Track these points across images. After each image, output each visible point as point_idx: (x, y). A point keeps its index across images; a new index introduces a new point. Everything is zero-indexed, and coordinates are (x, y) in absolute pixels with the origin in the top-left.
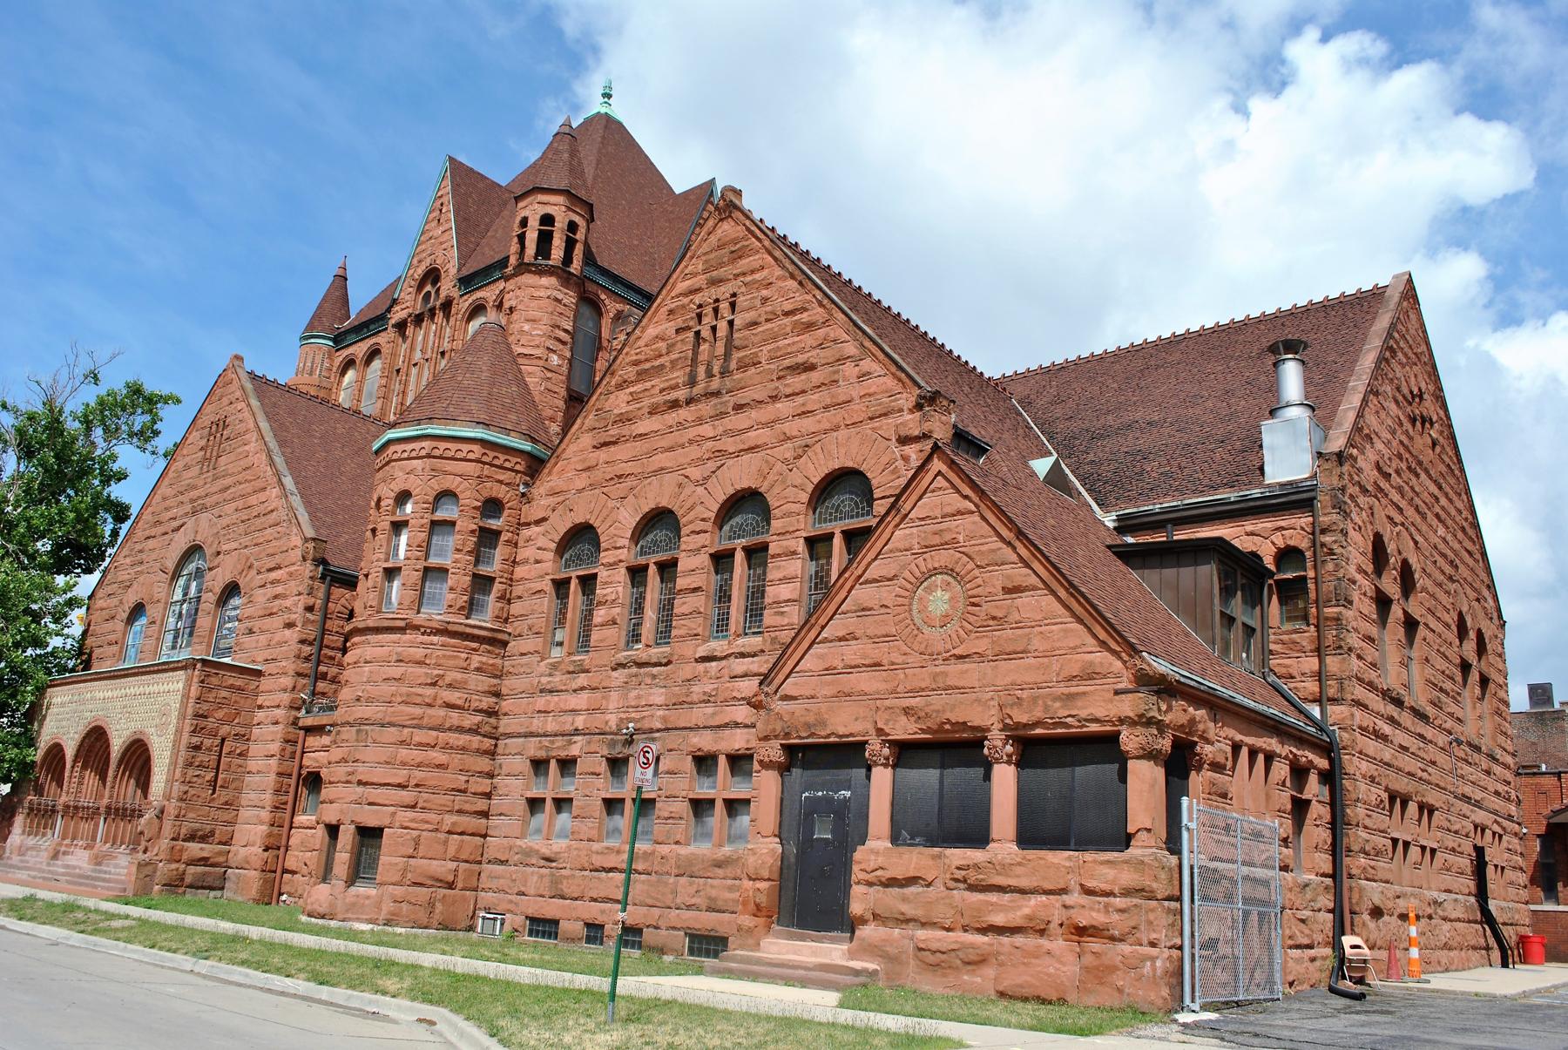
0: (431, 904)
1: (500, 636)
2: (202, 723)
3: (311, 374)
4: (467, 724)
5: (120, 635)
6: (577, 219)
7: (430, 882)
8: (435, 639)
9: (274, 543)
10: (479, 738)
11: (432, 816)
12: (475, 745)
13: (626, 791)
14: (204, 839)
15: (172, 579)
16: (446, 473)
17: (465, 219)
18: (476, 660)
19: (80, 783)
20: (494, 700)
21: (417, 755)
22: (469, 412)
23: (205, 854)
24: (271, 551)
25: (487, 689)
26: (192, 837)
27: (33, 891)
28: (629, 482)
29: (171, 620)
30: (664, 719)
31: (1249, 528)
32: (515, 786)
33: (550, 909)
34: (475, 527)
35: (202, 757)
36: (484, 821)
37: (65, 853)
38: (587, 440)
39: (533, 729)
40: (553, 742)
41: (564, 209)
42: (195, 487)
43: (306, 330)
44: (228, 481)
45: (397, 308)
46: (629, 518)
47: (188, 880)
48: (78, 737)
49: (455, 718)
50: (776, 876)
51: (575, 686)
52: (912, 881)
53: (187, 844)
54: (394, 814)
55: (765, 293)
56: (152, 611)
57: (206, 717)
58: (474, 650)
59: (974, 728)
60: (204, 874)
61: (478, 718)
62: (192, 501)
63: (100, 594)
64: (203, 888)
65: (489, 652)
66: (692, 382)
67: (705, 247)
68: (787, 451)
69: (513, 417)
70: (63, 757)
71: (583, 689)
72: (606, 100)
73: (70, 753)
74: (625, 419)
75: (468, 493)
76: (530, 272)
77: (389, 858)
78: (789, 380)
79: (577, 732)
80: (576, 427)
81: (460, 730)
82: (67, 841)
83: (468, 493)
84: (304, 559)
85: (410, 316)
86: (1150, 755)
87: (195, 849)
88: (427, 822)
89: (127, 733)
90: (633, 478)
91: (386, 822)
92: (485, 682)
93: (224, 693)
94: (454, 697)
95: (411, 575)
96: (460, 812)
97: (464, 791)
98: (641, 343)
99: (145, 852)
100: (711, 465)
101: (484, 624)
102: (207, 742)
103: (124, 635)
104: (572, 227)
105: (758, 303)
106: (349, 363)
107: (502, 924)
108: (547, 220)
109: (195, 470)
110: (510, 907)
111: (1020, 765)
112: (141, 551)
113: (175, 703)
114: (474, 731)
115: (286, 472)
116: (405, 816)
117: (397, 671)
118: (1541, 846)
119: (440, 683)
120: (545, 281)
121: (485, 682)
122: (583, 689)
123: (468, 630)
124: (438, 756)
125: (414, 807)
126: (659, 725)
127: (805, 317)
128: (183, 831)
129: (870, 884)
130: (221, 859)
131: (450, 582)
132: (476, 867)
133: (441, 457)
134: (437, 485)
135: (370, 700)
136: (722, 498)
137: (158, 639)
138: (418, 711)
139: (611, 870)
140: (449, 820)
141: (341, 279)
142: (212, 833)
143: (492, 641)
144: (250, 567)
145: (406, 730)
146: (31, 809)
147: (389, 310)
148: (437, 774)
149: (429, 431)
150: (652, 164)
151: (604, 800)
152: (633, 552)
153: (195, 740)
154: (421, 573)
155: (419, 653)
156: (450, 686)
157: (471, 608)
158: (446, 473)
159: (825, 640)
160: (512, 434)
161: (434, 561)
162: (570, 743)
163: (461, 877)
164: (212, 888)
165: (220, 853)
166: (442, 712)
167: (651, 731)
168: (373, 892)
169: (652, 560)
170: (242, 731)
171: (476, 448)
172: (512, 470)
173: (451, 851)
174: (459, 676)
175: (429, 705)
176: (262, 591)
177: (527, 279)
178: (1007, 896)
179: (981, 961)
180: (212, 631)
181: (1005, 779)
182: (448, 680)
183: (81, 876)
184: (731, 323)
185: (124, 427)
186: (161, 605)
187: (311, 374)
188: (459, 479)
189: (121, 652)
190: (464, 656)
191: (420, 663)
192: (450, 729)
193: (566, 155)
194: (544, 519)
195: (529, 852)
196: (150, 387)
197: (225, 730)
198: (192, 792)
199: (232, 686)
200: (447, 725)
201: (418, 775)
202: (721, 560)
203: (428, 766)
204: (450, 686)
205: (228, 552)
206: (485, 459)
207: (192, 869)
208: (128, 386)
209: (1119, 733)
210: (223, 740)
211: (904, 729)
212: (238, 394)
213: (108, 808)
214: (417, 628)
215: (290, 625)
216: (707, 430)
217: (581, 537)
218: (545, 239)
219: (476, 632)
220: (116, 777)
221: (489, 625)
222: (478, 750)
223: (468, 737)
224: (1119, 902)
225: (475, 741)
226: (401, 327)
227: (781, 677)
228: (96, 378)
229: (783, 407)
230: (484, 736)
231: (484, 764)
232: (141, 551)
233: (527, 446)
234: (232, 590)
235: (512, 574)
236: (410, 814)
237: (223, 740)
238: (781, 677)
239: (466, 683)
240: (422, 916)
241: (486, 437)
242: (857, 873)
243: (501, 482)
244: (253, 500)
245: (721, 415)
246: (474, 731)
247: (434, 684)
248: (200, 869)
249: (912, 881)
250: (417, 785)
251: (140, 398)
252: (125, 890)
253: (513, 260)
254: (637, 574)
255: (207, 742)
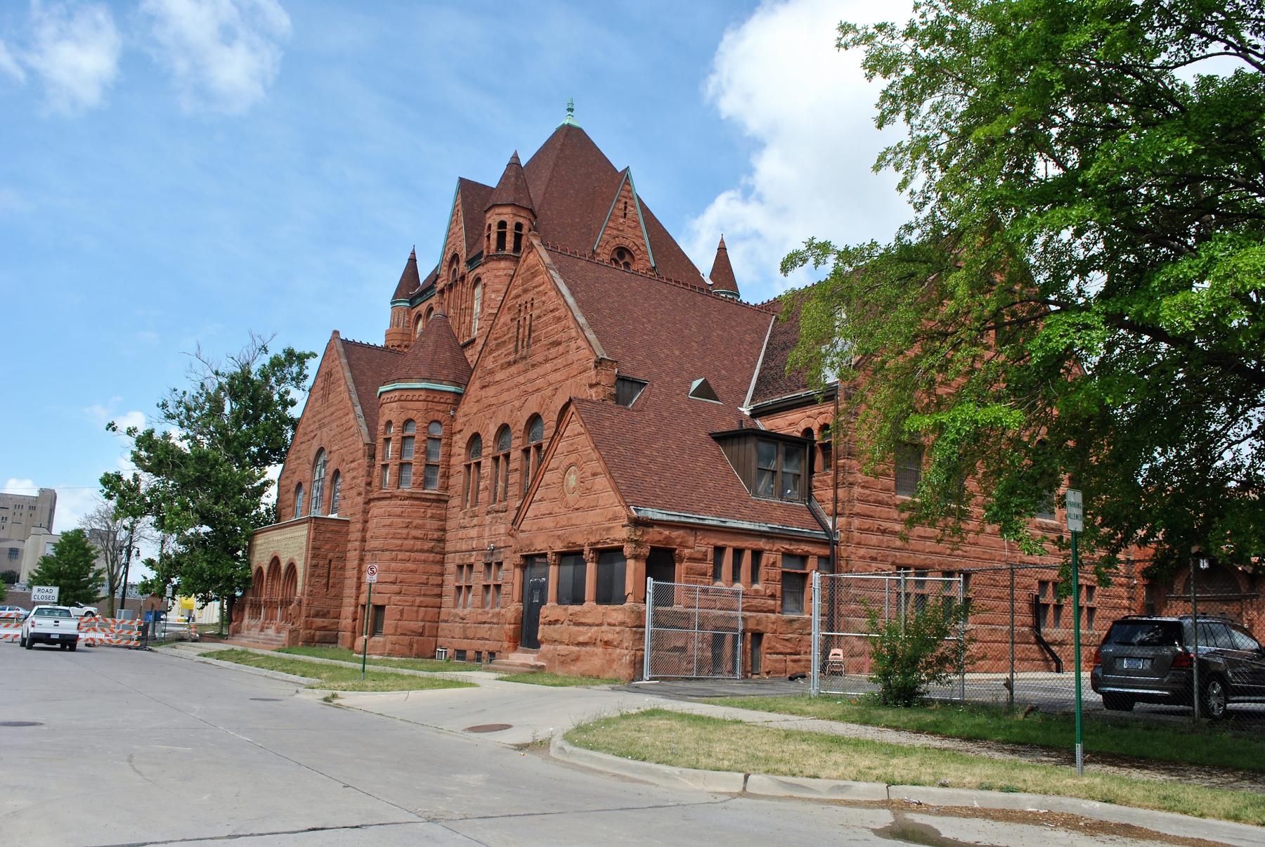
0: (411, 645)
1: (442, 498)
2: (318, 552)
3: (398, 326)
4: (426, 547)
5: (292, 501)
6: (521, 220)
7: (409, 633)
8: (407, 502)
9: (353, 446)
10: (433, 554)
11: (409, 598)
12: (431, 559)
13: (491, 582)
14: (324, 616)
15: (313, 467)
16: (408, 409)
17: (471, 219)
18: (429, 512)
19: (272, 588)
20: (442, 533)
21: (400, 566)
22: (419, 373)
23: (325, 624)
24: (351, 451)
25: (436, 527)
26: (317, 615)
27: (233, 646)
28: (494, 408)
29: (315, 491)
30: (504, 541)
31: (808, 413)
32: (451, 581)
33: (464, 645)
34: (425, 438)
35: (319, 571)
36: (439, 600)
37: (267, 628)
38: (477, 384)
39: (457, 549)
40: (464, 555)
41: (511, 216)
42: (320, 413)
43: (393, 299)
44: (332, 409)
45: (439, 281)
46: (493, 429)
47: (317, 638)
48: (268, 562)
49: (419, 544)
50: (519, 622)
51: (472, 525)
52: (556, 622)
53: (314, 619)
54: (390, 598)
55: (544, 298)
56: (305, 487)
57: (319, 549)
58: (429, 506)
59: (580, 545)
60: (325, 635)
61: (433, 544)
62: (319, 421)
63: (283, 477)
64: (325, 643)
65: (437, 507)
66: (516, 351)
67: (522, 271)
68: (548, 392)
69: (445, 372)
70: (262, 572)
71: (475, 526)
72: (570, 113)
73: (265, 571)
74: (491, 372)
75: (420, 420)
76: (493, 260)
77: (388, 622)
78: (552, 350)
79: (473, 550)
80: (473, 376)
81: (422, 551)
82: (268, 621)
83: (420, 420)
84: (364, 456)
85: (445, 285)
86: (636, 557)
87: (319, 622)
88: (406, 601)
89: (287, 559)
90: (494, 407)
91: (386, 602)
92: (436, 524)
93: (328, 535)
94: (418, 533)
95: (393, 468)
96: (424, 595)
97: (427, 584)
98: (498, 327)
99: (293, 624)
100: (523, 399)
101: (433, 492)
102: (321, 563)
103: (294, 501)
104: (519, 226)
105: (541, 304)
106: (419, 317)
107: (446, 654)
108: (502, 224)
109: (319, 402)
110: (450, 645)
111: (598, 562)
112: (299, 451)
113: (304, 540)
114: (431, 551)
115: (358, 404)
116: (396, 598)
117: (388, 521)
118: (1147, 593)
119: (410, 526)
120: (503, 264)
121: (436, 524)
122: (475, 526)
123: (423, 496)
124: (410, 566)
125: (400, 593)
126: (503, 545)
127: (557, 314)
128: (312, 612)
129: (545, 624)
130: (335, 627)
131: (413, 470)
132: (436, 624)
133: (405, 401)
134: (404, 417)
135: (377, 538)
136: (526, 418)
137: (308, 503)
138: (399, 542)
139: (484, 623)
140: (418, 600)
141: (413, 261)
142: (328, 612)
143: (439, 501)
144: (343, 461)
145: (394, 553)
146: (252, 604)
147: (435, 282)
148: (410, 575)
149: (397, 387)
150: (602, 154)
151: (484, 585)
152: (496, 449)
153: (314, 562)
154: (398, 467)
155: (399, 510)
156: (415, 527)
157: (426, 483)
158: (408, 409)
159: (535, 501)
160: (444, 382)
161: (406, 459)
162: (471, 555)
163: (426, 630)
164: (330, 643)
165: (334, 624)
166: (412, 542)
167: (500, 548)
168: (381, 639)
169: (502, 452)
170: (341, 555)
171: (422, 393)
172: (445, 403)
173: (421, 615)
174: (420, 522)
175: (405, 538)
176: (348, 474)
177: (492, 265)
178: (586, 628)
179: (577, 659)
180: (330, 499)
181: (591, 569)
182: (414, 524)
183: (270, 639)
184: (531, 315)
185: (288, 376)
186: (308, 483)
187: (398, 326)
188: (415, 412)
189: (293, 511)
190: (423, 510)
191: (399, 516)
192: (417, 551)
193: (513, 179)
194: (461, 431)
195: (456, 615)
196: (298, 350)
197: (331, 555)
198: (315, 591)
199: (332, 531)
200: (415, 549)
201: (401, 576)
202: (526, 451)
203: (406, 571)
204: (415, 527)
205: (335, 451)
206: (429, 399)
207: (318, 633)
208: (284, 352)
209: (623, 546)
210: (330, 561)
211: (559, 547)
212: (336, 355)
213: (282, 601)
214: (397, 497)
215: (359, 494)
216: (521, 379)
217: (476, 438)
218: (501, 237)
219: (428, 497)
220: (284, 584)
221: (436, 492)
222: (433, 562)
223: (427, 555)
224: (618, 629)
225: (431, 556)
226: (442, 292)
227: (520, 521)
228: (265, 349)
229: (548, 366)
230: (437, 553)
231: (437, 569)
232: (299, 451)
233: (452, 389)
234: (337, 473)
235: (449, 461)
236: (398, 598)
237: (330, 561)
238: (520, 521)
239: (424, 525)
240: (406, 651)
241: (427, 387)
242: (541, 620)
243: (439, 411)
244: (344, 421)
245: (526, 371)
246: (431, 551)
247: (407, 527)
248: (322, 633)
249: (556, 622)
250: (401, 582)
251: (294, 358)
252: (284, 645)
253: (485, 253)
254: (496, 459)
255: (321, 563)
